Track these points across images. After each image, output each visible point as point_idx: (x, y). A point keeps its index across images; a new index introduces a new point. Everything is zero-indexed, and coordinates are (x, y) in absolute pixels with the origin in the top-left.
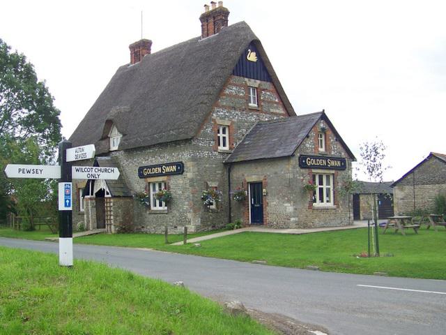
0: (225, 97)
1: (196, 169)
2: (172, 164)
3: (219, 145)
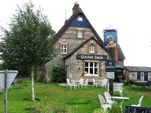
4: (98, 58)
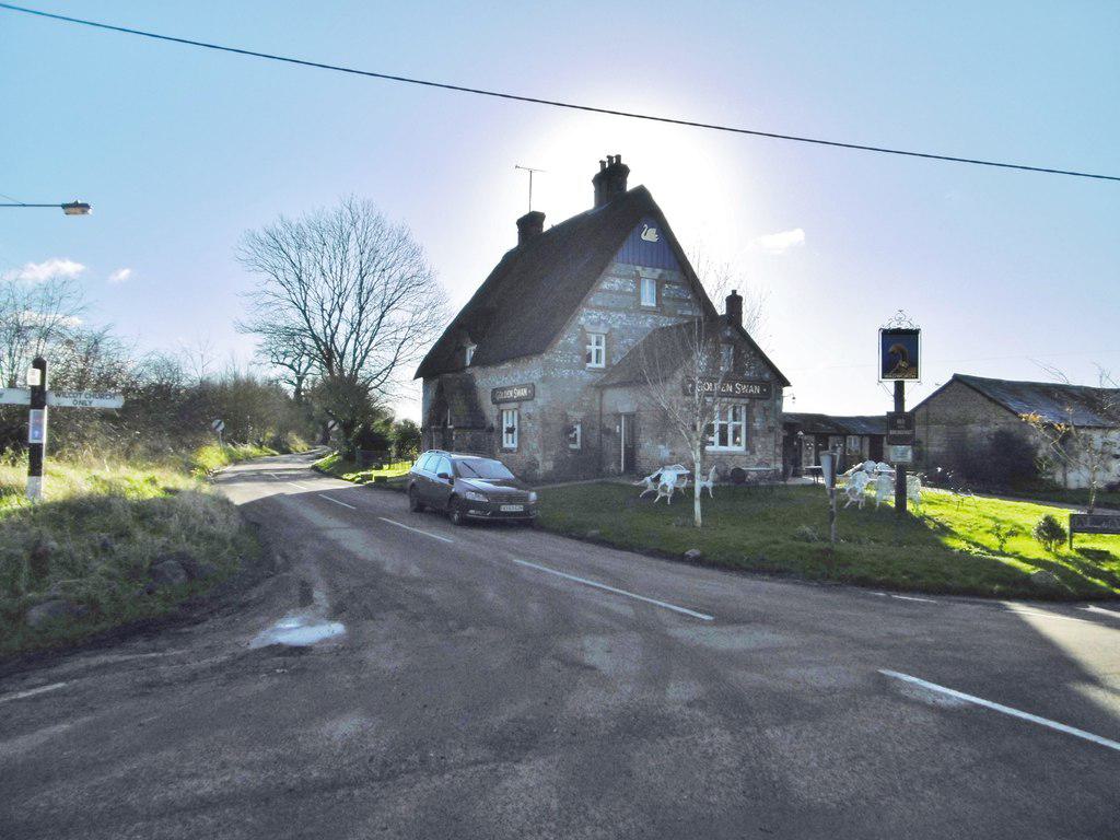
2: (521, 387)
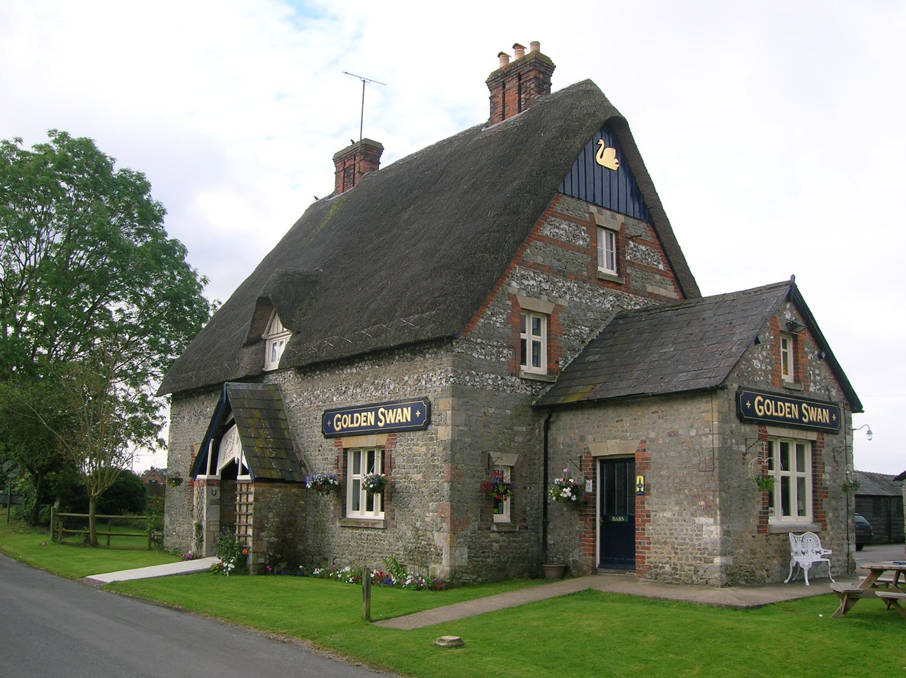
0: (539, 243)
1: (461, 419)
3: (523, 362)
4: (405, 409)
